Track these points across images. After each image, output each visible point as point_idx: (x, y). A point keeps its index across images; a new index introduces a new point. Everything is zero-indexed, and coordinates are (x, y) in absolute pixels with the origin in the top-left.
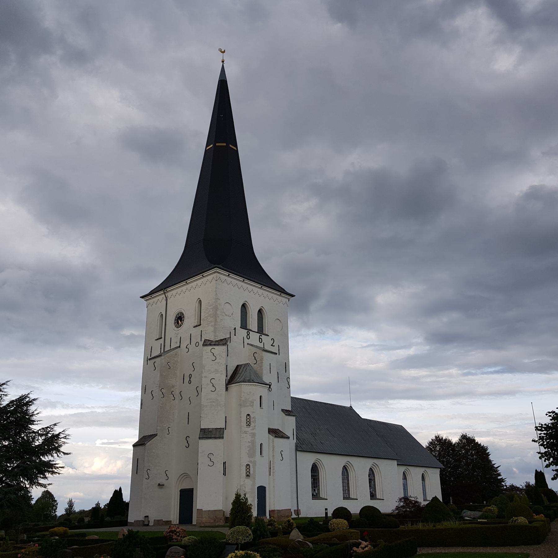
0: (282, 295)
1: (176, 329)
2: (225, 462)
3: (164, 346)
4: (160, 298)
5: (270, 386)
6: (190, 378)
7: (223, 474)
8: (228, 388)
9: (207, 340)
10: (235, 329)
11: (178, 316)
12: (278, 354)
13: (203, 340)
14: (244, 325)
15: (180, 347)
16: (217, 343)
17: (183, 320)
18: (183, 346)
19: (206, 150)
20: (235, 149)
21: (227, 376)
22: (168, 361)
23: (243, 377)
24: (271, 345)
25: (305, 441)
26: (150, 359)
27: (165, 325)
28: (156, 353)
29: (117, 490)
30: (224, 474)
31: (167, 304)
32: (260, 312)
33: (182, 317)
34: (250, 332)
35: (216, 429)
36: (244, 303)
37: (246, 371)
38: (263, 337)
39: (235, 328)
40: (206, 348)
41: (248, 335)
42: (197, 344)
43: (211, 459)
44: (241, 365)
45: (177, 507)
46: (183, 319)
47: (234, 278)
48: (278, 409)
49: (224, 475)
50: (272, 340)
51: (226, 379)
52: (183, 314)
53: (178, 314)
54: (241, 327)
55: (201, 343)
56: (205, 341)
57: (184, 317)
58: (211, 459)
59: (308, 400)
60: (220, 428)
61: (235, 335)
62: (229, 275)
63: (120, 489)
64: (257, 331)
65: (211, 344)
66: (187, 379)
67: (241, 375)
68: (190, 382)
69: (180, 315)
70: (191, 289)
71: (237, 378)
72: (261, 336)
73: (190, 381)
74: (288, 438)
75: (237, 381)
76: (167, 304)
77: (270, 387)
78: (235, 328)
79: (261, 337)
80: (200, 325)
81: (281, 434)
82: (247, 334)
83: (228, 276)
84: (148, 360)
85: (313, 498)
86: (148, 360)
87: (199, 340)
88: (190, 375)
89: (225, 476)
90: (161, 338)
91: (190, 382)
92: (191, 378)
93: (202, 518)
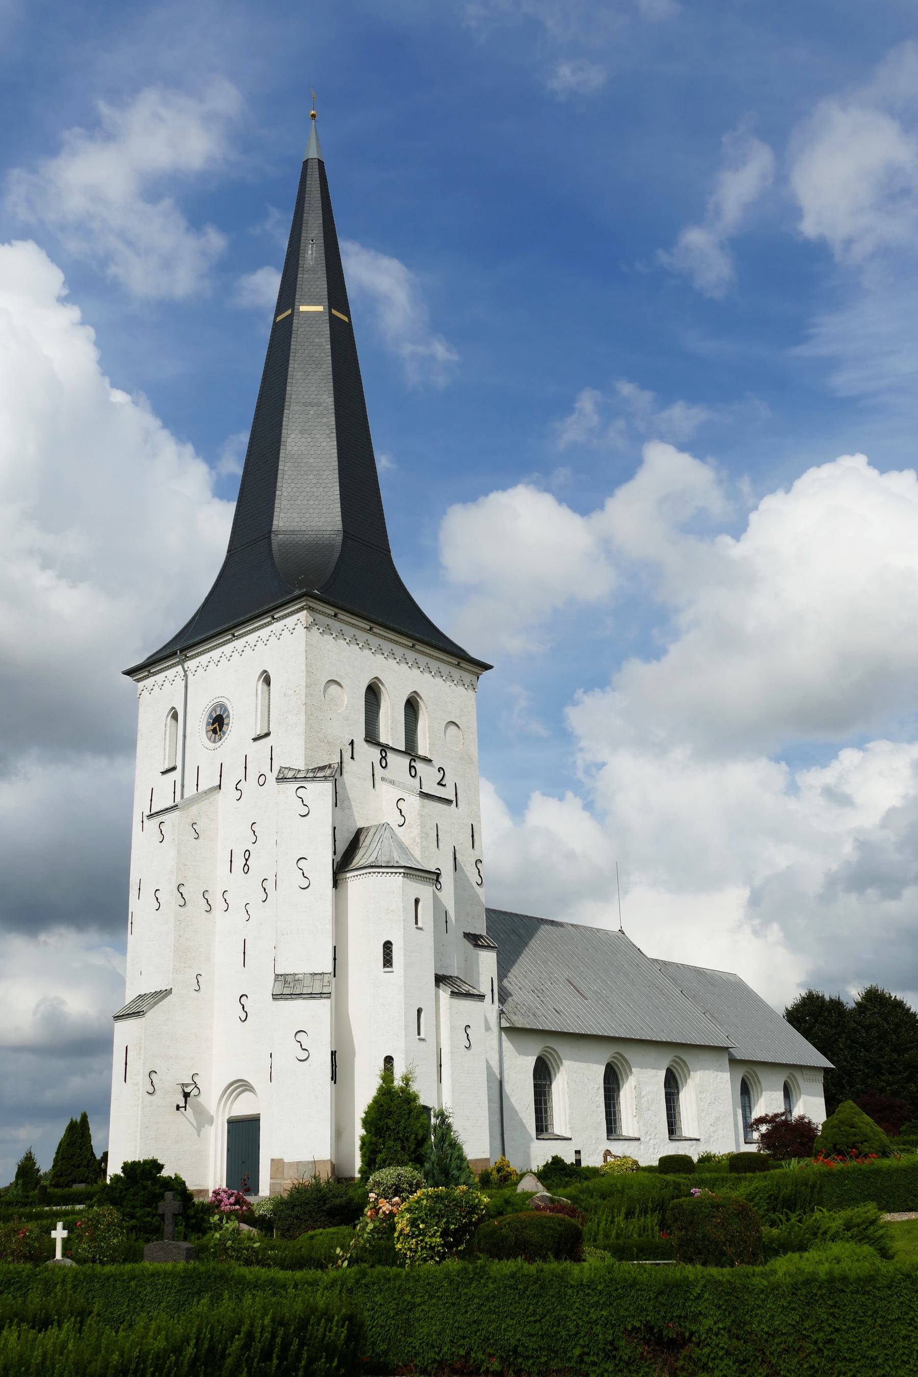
0: (375, 630)
1: (212, 745)
2: (335, 1052)
3: (183, 786)
4: (171, 673)
5: (438, 875)
6: (247, 860)
7: (330, 1079)
8: (339, 882)
9: (285, 768)
10: (352, 743)
11: (214, 716)
12: (454, 803)
13: (276, 769)
14: (372, 738)
15: (220, 788)
16: (311, 775)
17: (228, 724)
18: (228, 784)
19: (275, 324)
20: (346, 319)
21: (335, 853)
22: (192, 819)
23: (375, 855)
24: (439, 784)
25: (519, 1007)
26: (151, 816)
27: (185, 736)
28: (280, 777)
29: (76, 1122)
30: (332, 1079)
31: (186, 687)
32: (412, 706)
33: (224, 716)
34: (387, 751)
35: (311, 974)
36: (373, 681)
37: (381, 840)
38: (419, 765)
39: (352, 740)
40: (284, 786)
41: (383, 757)
42: (262, 779)
43: (301, 1045)
44: (368, 829)
45: (222, 1163)
46: (226, 721)
47: (383, 636)
48: (456, 934)
49: (333, 1081)
50: (439, 771)
51: (333, 860)
52: (226, 710)
53: (214, 710)
54: (368, 739)
55: (272, 777)
56: (280, 769)
57: (228, 716)
58: (301, 1045)
59: (522, 915)
60: (321, 974)
61: (352, 758)
62: (459, 663)
63: (84, 1117)
64: (404, 749)
65: (296, 778)
66: (239, 862)
67: (369, 852)
68: (246, 868)
69: (218, 713)
70: (245, 649)
71: (360, 859)
72: (412, 762)
73: (246, 867)
74: (481, 997)
75: (360, 864)
76: (186, 687)
77: (437, 880)
78: (352, 740)
79: (413, 764)
80: (267, 735)
81: (464, 988)
82: (381, 754)
83: (458, 665)
84: (145, 818)
85: (539, 1137)
86: (145, 818)
87: (266, 770)
88: (247, 853)
89: (335, 1083)
90: (174, 769)
91: (246, 868)
92: (249, 859)
93: (283, 1178)
